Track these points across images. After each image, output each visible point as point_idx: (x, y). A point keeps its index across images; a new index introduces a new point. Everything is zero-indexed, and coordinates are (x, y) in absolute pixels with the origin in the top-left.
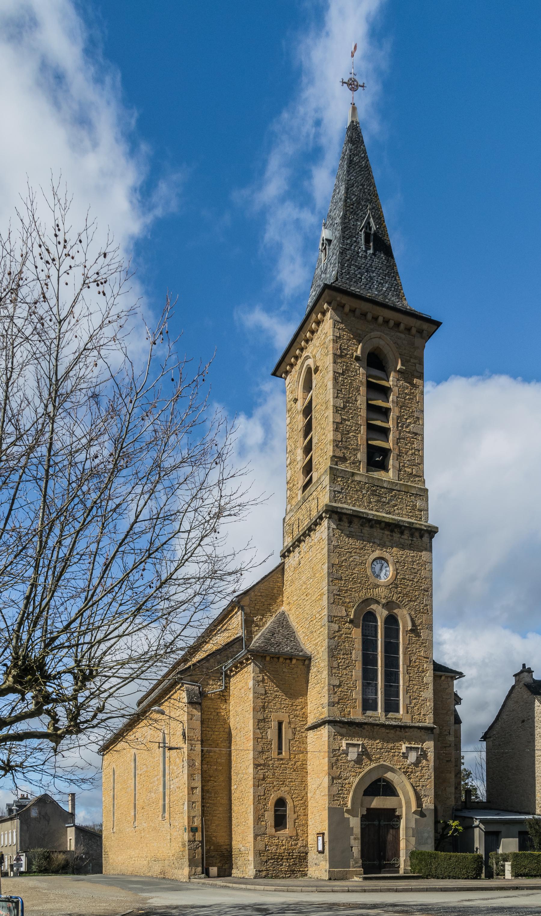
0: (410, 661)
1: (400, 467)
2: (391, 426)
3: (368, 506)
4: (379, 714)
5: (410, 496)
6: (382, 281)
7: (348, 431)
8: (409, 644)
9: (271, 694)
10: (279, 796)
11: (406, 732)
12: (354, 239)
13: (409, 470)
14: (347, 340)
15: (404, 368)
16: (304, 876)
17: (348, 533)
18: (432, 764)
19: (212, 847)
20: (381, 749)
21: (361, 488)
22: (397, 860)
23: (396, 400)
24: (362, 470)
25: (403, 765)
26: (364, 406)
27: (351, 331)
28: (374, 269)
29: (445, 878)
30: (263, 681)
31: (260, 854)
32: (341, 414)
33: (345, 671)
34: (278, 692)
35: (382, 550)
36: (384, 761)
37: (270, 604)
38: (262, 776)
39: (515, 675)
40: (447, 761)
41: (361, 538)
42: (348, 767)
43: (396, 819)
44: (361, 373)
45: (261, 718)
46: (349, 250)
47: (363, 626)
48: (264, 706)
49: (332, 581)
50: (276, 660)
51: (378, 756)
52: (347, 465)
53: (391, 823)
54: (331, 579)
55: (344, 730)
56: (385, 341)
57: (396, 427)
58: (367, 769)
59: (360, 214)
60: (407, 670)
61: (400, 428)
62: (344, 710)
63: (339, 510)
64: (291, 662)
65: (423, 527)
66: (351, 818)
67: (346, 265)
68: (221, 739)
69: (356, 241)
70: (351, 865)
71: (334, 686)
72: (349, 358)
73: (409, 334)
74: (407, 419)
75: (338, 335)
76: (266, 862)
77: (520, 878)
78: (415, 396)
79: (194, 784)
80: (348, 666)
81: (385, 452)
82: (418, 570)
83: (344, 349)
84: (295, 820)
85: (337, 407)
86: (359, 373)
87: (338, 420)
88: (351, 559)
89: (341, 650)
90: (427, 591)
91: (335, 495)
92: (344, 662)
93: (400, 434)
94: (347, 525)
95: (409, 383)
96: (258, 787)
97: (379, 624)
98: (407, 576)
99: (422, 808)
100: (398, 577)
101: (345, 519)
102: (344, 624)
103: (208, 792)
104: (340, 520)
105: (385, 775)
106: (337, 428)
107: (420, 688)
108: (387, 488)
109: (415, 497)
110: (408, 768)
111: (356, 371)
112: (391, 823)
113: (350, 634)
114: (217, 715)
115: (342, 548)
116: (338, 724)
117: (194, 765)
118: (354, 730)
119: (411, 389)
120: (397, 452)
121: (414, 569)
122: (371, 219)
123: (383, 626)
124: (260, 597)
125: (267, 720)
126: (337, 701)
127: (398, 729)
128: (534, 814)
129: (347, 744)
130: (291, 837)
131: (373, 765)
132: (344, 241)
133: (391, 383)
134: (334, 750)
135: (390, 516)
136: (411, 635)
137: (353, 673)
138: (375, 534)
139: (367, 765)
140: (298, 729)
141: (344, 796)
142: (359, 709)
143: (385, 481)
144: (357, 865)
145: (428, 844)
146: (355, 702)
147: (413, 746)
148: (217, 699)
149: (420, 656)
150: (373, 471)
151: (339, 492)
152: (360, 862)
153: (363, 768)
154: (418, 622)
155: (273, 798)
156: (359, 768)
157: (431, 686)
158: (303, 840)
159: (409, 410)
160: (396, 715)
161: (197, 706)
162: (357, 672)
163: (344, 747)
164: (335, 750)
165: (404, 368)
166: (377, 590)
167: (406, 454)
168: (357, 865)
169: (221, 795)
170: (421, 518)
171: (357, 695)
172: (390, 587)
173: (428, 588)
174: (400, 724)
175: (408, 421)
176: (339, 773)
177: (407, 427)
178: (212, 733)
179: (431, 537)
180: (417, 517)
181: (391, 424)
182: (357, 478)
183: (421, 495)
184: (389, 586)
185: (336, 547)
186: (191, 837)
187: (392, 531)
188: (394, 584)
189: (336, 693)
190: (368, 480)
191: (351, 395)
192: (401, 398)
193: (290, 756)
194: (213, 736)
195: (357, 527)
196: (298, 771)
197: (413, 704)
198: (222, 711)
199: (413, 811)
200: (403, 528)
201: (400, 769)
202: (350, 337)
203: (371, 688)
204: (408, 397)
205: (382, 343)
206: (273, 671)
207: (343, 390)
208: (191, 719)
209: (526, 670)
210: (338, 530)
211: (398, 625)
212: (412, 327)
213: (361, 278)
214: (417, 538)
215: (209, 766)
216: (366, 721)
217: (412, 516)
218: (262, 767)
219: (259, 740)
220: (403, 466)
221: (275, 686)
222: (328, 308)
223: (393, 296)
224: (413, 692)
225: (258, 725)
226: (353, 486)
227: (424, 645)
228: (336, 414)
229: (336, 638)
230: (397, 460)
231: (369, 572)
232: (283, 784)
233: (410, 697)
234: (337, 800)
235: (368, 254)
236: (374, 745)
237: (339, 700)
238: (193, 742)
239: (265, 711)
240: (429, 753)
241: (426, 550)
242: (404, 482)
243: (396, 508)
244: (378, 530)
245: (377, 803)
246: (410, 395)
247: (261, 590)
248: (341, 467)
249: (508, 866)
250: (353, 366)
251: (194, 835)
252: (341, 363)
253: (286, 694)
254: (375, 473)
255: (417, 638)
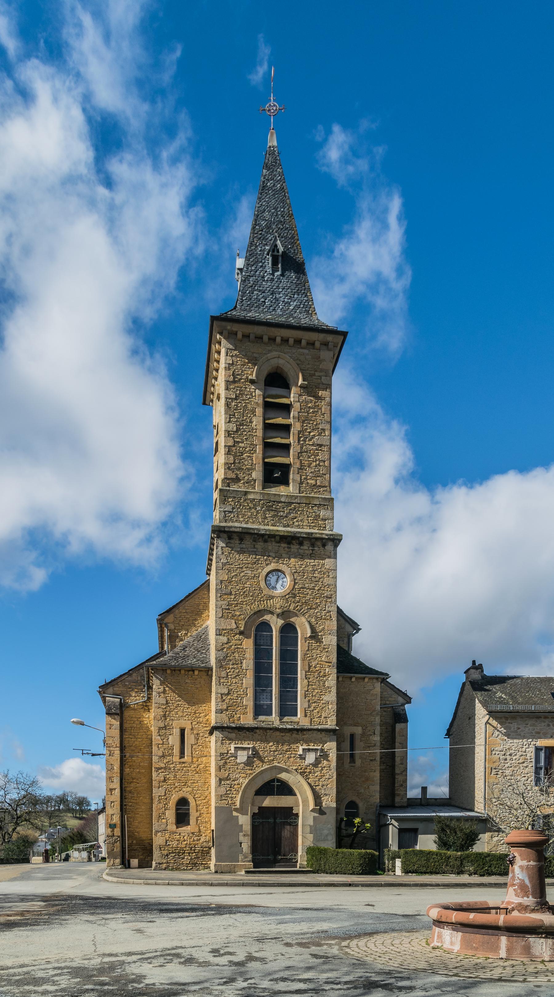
0: (310, 667)
1: (301, 479)
2: (292, 442)
3: (263, 522)
4: (274, 719)
5: (312, 507)
6: (289, 301)
7: (242, 453)
8: (308, 650)
9: (173, 703)
10: (181, 796)
11: (304, 735)
12: (261, 264)
13: (313, 482)
14: (241, 365)
15: (306, 383)
16: (207, 868)
17: (239, 549)
18: (334, 764)
19: (134, 842)
20: (274, 751)
21: (255, 505)
22: (295, 856)
23: (297, 416)
24: (258, 487)
25: (300, 765)
26: (260, 427)
27: (245, 356)
28: (280, 290)
29: (333, 873)
30: (164, 692)
31: (160, 848)
32: (233, 437)
33: (234, 680)
34: (180, 701)
35: (277, 562)
36: (279, 763)
37: (195, 620)
38: (162, 778)
39: (465, 673)
40: (371, 760)
41: (254, 553)
42: (237, 769)
43: (293, 817)
44: (257, 395)
45: (162, 725)
46: (252, 276)
47: (256, 635)
48: (165, 715)
49: (221, 596)
50: (178, 672)
51: (272, 758)
52: (240, 485)
53: (289, 821)
54: (219, 595)
55: (233, 735)
56: (283, 360)
57: (297, 441)
58: (258, 770)
59: (270, 238)
60: (306, 675)
61: (302, 442)
62: (234, 716)
63: (226, 529)
64: (194, 673)
65: (324, 536)
66: (240, 816)
67: (248, 292)
68: (144, 745)
69: (262, 266)
70: (240, 859)
71: (222, 694)
72: (243, 382)
73: (314, 349)
74: (310, 432)
75: (231, 362)
76: (167, 855)
77: (410, 874)
78: (321, 409)
79: (112, 786)
80: (238, 675)
81: (285, 468)
82: (320, 578)
83: (238, 375)
84: (198, 817)
85: (229, 431)
86: (255, 396)
87: (231, 443)
88: (242, 574)
89: (231, 660)
90: (331, 598)
91: (225, 515)
92: (234, 672)
93: (302, 448)
94: (238, 542)
95: (313, 396)
96: (159, 788)
97: (274, 633)
98: (307, 585)
99: (321, 806)
100: (296, 587)
101: (235, 536)
102: (234, 636)
103: (130, 792)
104: (230, 538)
105: (279, 776)
106: (229, 451)
107: (321, 692)
108: (284, 502)
109: (318, 507)
110: (306, 769)
111: (251, 394)
112: (289, 821)
113: (241, 645)
114: (140, 723)
115: (232, 564)
116: (227, 730)
117: (112, 768)
118: (244, 734)
119: (315, 402)
120: (298, 465)
121: (315, 577)
122: (279, 241)
123: (278, 635)
124: (185, 614)
125: (168, 727)
126: (225, 708)
127: (296, 732)
128: (472, 810)
129: (235, 748)
130: (193, 833)
131: (266, 766)
132: (248, 268)
133: (292, 399)
134: (222, 754)
135: (289, 529)
136: (311, 642)
137: (244, 681)
138: (270, 548)
139: (259, 767)
140: (201, 734)
141: (233, 796)
142: (250, 715)
143: (282, 495)
144: (246, 859)
145: (328, 840)
146: (245, 708)
147: (311, 747)
148: (140, 709)
149: (321, 661)
150: (271, 487)
151: (230, 512)
152: (250, 857)
153: (255, 769)
154: (319, 628)
155: (174, 798)
156: (249, 770)
157: (334, 690)
158: (206, 836)
159: (313, 423)
160: (294, 719)
161: (116, 717)
162: (249, 680)
163: (232, 751)
164: (223, 754)
165: (306, 383)
166: (272, 601)
167: (309, 467)
168: (246, 859)
169: (144, 795)
170: (325, 527)
171: (249, 701)
172: (287, 597)
173: (332, 595)
174: (296, 727)
175: (312, 434)
176: (227, 775)
177: (310, 440)
178: (135, 739)
179: (336, 546)
180: (320, 527)
181: (292, 440)
182: (251, 496)
183: (325, 505)
184: (285, 596)
185: (224, 564)
186: (110, 832)
187: (289, 543)
188: (292, 594)
189: (224, 700)
190: (263, 497)
191: (245, 418)
192: (304, 412)
193: (192, 760)
194: (136, 743)
195: (249, 543)
196: (201, 773)
197: (312, 707)
198: (144, 719)
199: (311, 809)
200: (301, 539)
201: (296, 770)
202: (244, 362)
203: (265, 694)
204: (311, 410)
205: (281, 362)
206: (174, 682)
207: (236, 414)
208: (110, 728)
209: (476, 667)
210: (227, 548)
211: (297, 633)
212: (315, 341)
213: (264, 302)
214: (319, 548)
215: (132, 770)
216: (256, 726)
217: (315, 526)
218: (163, 770)
219: (160, 746)
220: (306, 479)
221: (177, 696)
222: (220, 338)
223: (301, 313)
224: (312, 696)
225: (159, 732)
226: (246, 504)
227: (327, 650)
228: (228, 438)
229: (225, 650)
230: (298, 473)
231: (263, 584)
232: (185, 785)
233: (309, 701)
234: (225, 800)
235: (276, 276)
236: (267, 748)
237: (227, 707)
238: (112, 749)
239: (166, 719)
240: (331, 755)
241: (329, 557)
242: (306, 494)
243: (295, 520)
244: (274, 544)
245: (269, 802)
246: (314, 408)
247: (186, 608)
248: (234, 487)
249: (398, 863)
250: (248, 390)
251: (113, 831)
252: (234, 389)
253: (189, 703)
254: (273, 489)
255: (318, 644)
